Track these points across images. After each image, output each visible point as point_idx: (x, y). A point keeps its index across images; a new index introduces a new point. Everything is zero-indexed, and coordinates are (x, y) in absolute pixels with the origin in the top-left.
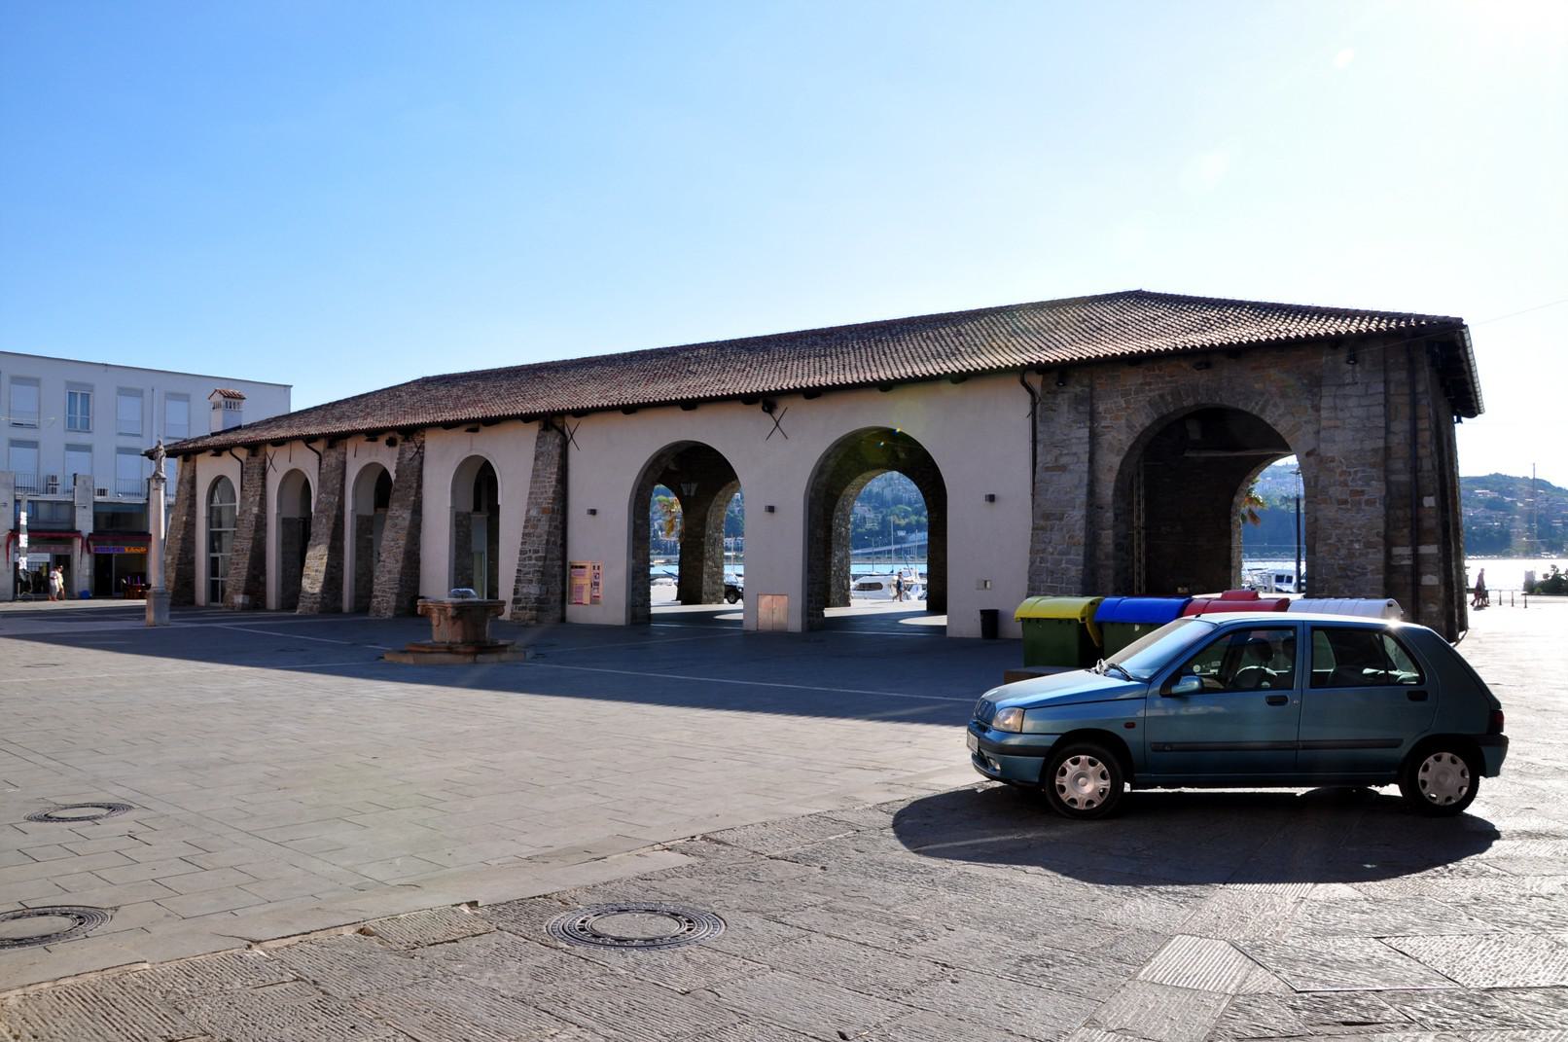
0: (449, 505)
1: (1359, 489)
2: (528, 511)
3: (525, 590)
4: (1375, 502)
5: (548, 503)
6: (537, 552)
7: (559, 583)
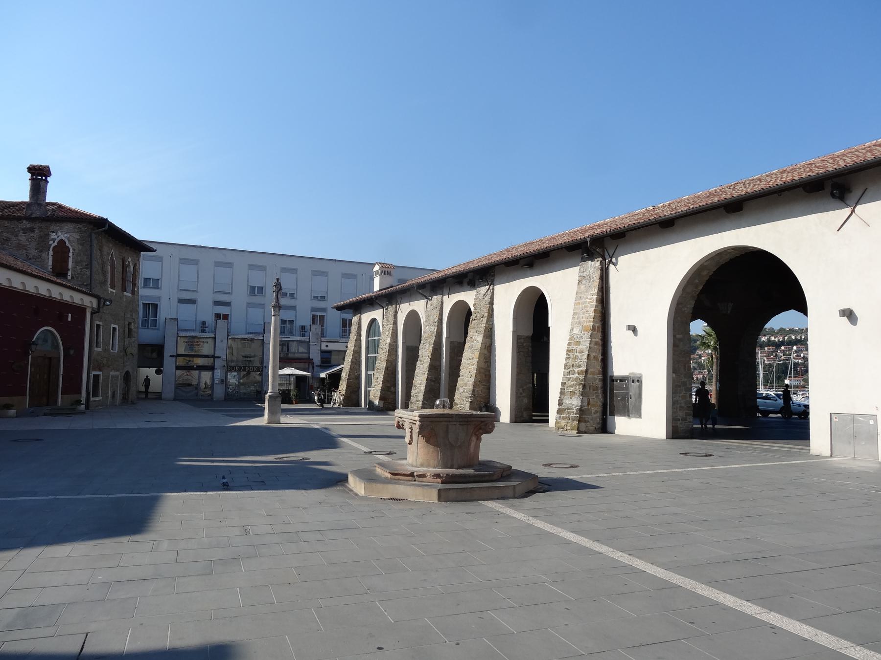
2: (572, 330)
5: (590, 321)
6: (579, 366)
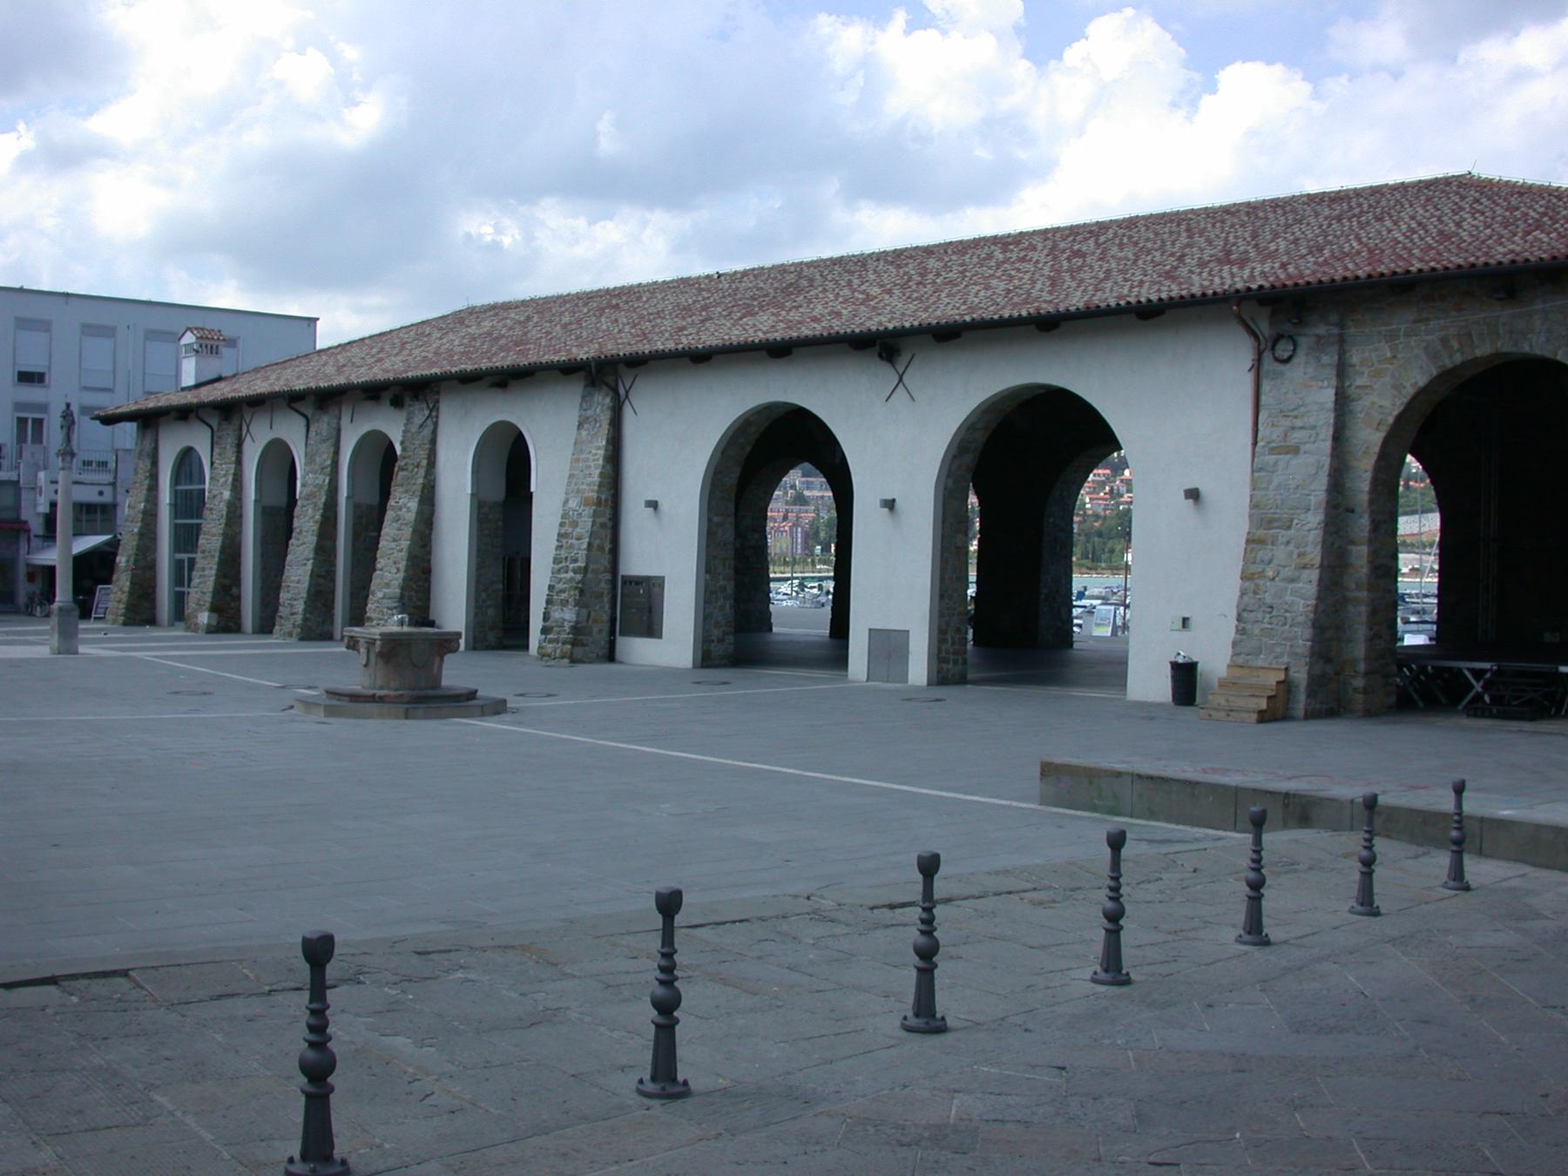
6: (576, 561)
7: (607, 606)
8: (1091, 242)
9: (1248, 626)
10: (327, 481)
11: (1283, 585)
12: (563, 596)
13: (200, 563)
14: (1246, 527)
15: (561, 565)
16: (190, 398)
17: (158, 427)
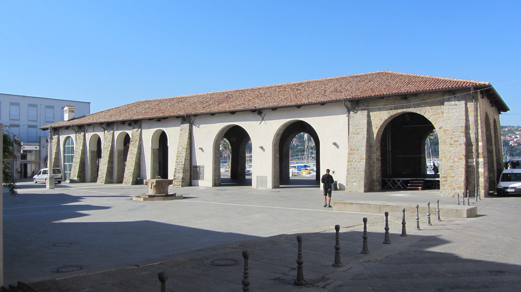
0: (151, 146)
1: (457, 140)
3: (177, 175)
4: (462, 144)
6: (182, 162)
7: (189, 173)
8: (300, 86)
9: (350, 173)
10: (111, 144)
11: (357, 163)
12: (179, 171)
13: (73, 166)
14: (347, 151)
15: (178, 164)
16: (69, 124)
17: (59, 131)
